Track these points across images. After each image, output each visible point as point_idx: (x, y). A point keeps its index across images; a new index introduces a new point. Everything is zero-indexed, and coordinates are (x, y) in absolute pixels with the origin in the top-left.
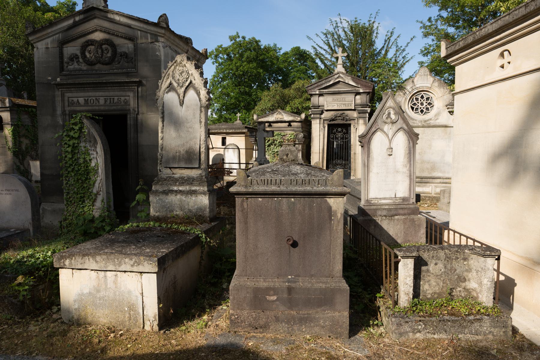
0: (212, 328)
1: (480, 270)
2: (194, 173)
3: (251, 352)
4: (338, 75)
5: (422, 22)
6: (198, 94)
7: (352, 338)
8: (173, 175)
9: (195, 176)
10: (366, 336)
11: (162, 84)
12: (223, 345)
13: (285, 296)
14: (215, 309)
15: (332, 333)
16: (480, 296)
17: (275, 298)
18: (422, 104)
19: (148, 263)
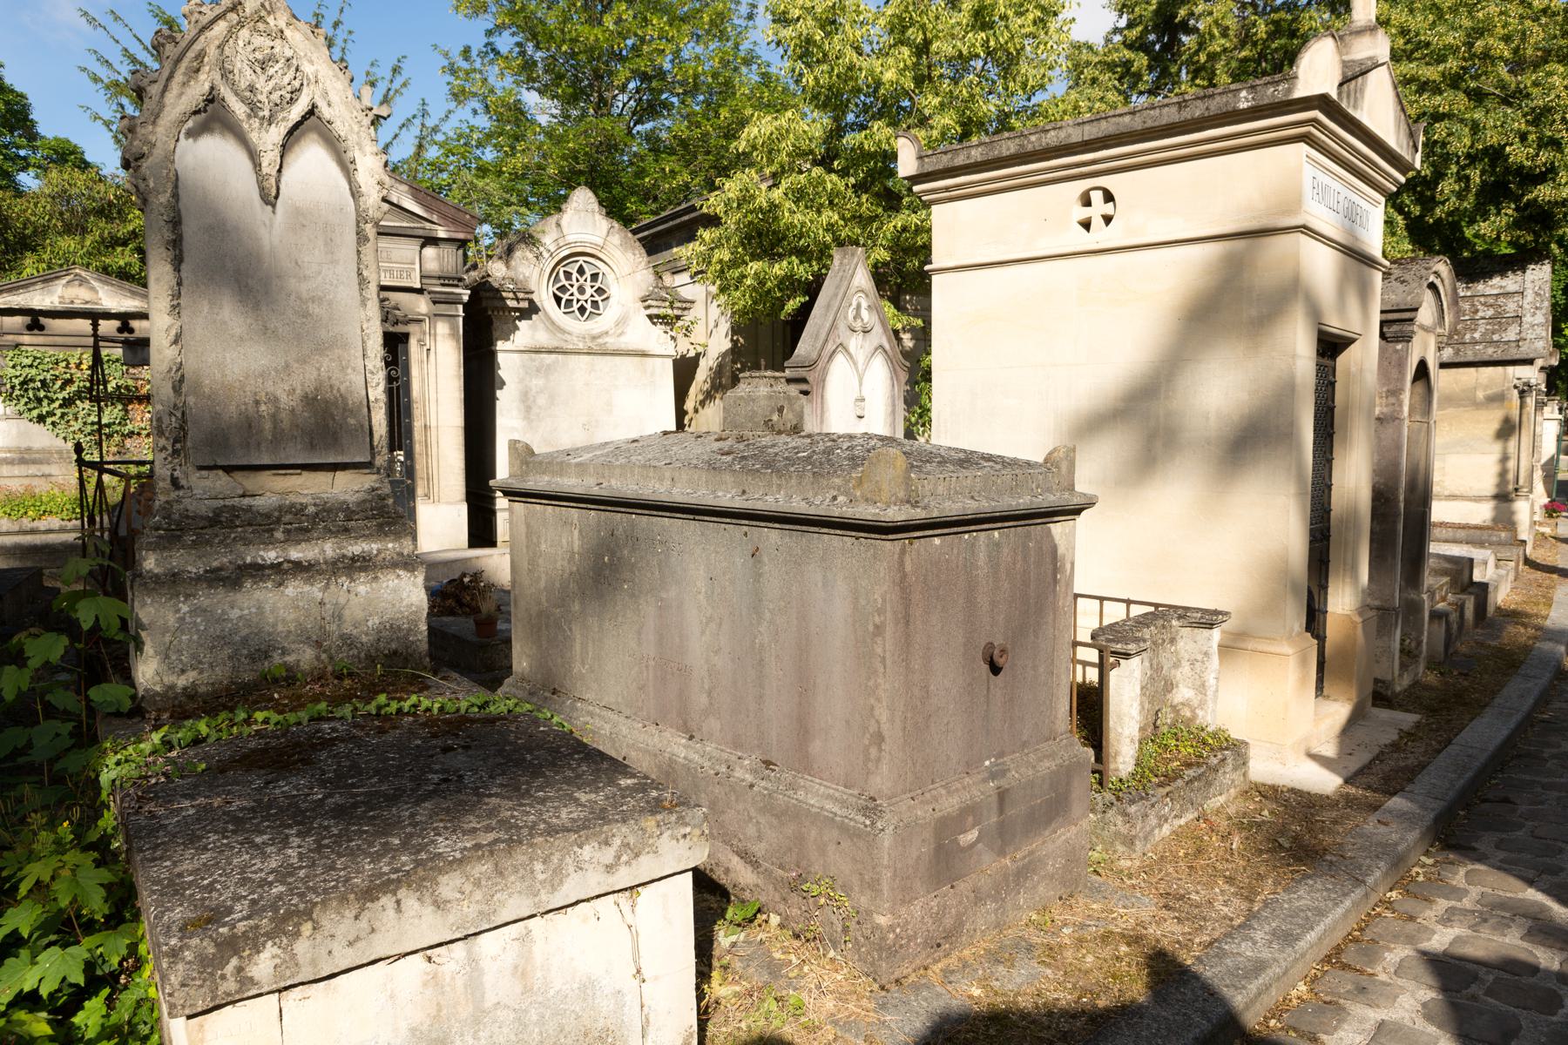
1: (1199, 657)
5: (446, 55)
8: (246, 501)
9: (351, 499)
11: (165, 89)
16: (1200, 713)
18: (581, 290)
19: (673, 837)
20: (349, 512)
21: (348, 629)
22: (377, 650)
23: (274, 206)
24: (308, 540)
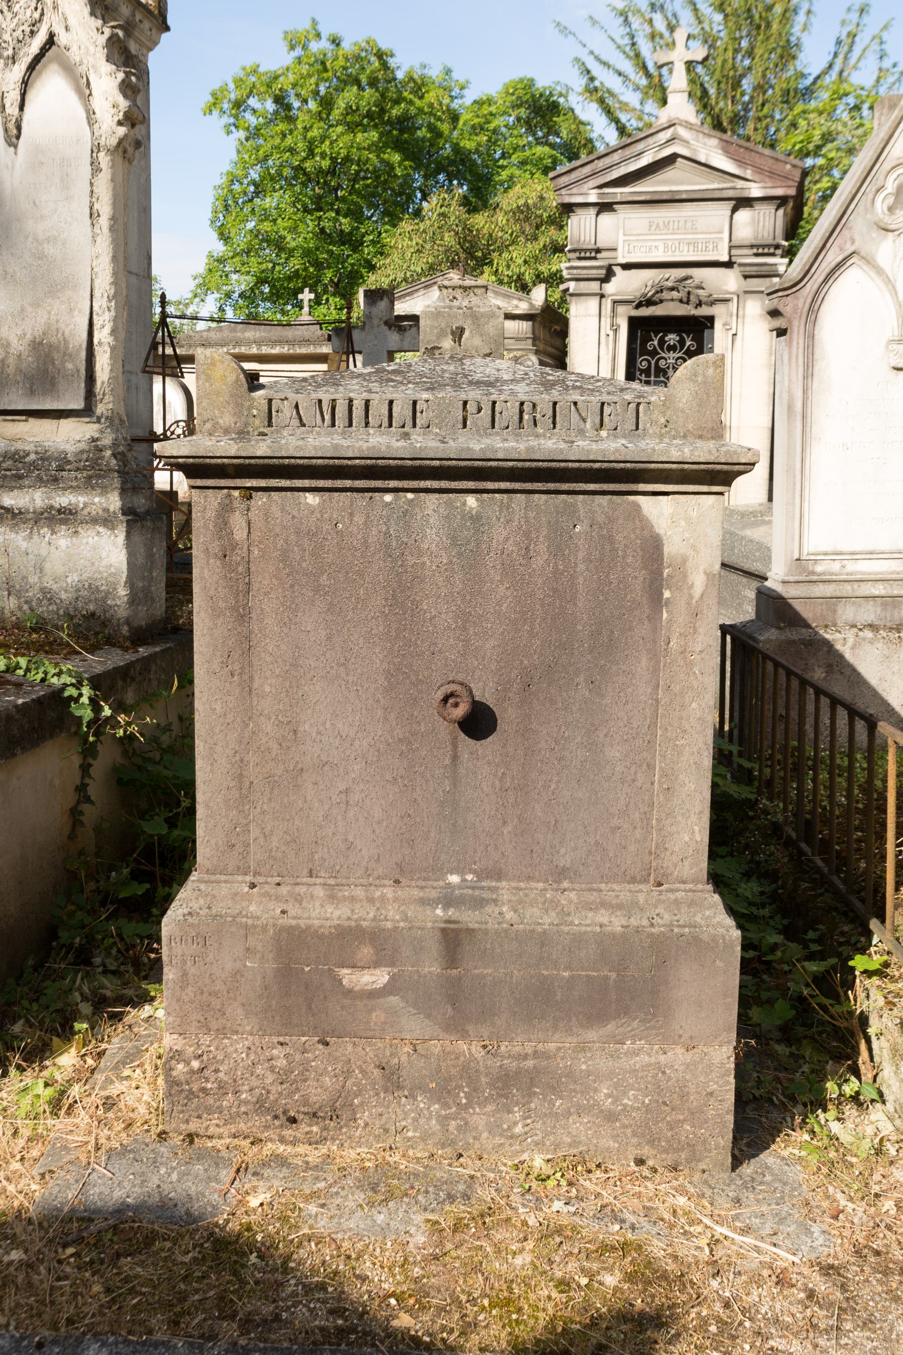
0: (82, 1118)
2: (69, 436)
3: (252, 1246)
4: (668, 134)
6: (84, 90)
7: (747, 1169)
9: (71, 449)
10: (813, 1159)
12: (121, 1210)
13: (432, 967)
14: (117, 1017)
15: (651, 1142)
17: (379, 978)
20: (63, 462)
21: (49, 583)
22: (76, 609)
23: (16, 147)
24: (21, 488)
